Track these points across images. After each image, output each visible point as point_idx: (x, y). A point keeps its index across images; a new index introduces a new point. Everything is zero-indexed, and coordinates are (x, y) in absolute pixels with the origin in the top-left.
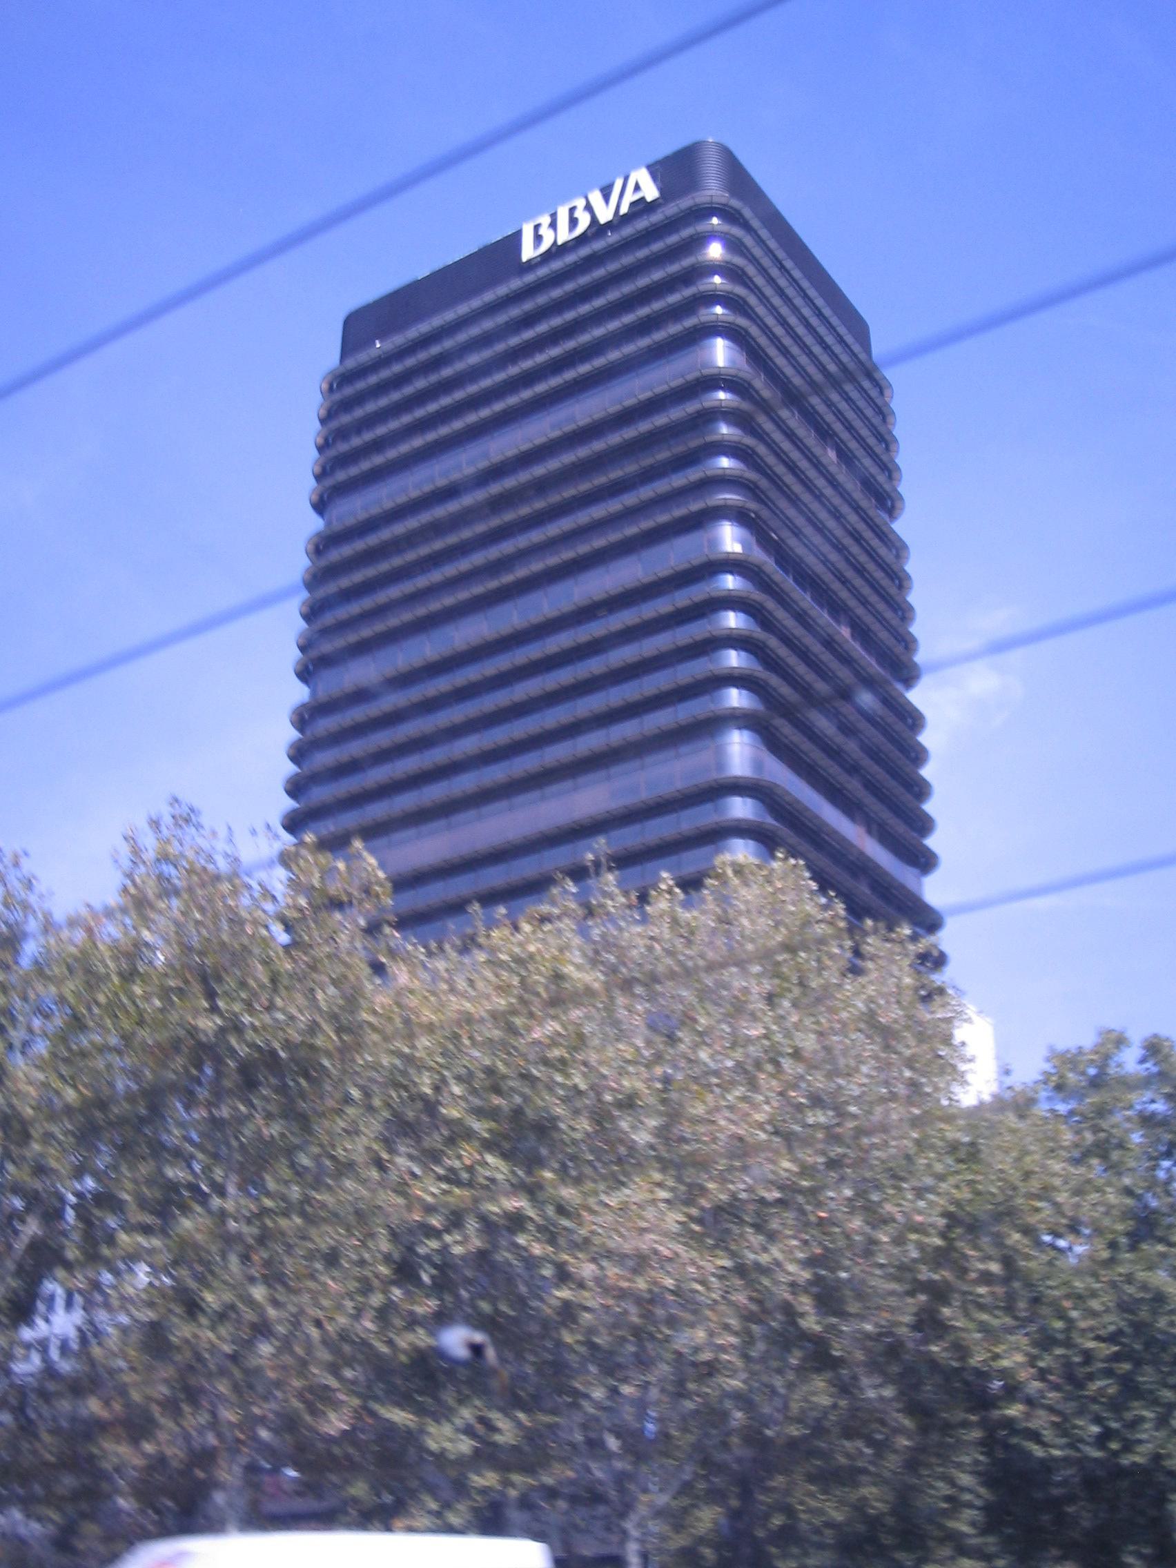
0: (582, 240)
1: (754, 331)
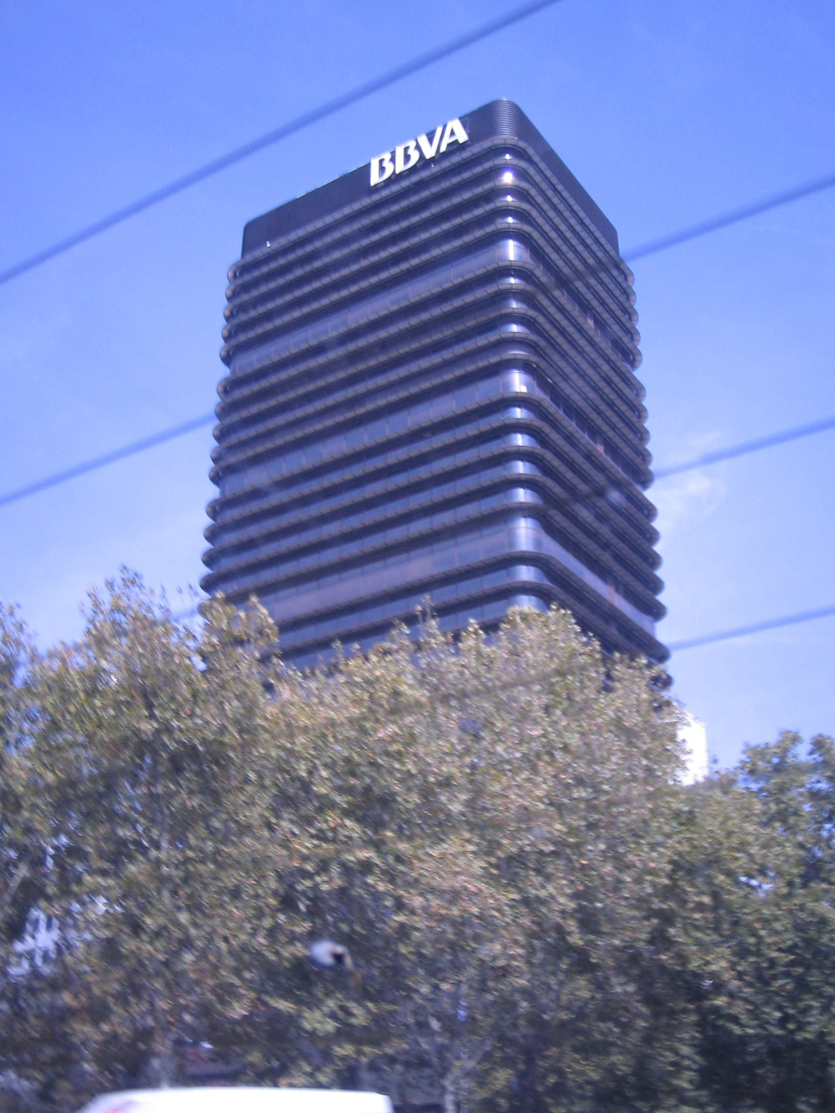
0: (413, 170)
1: (535, 235)
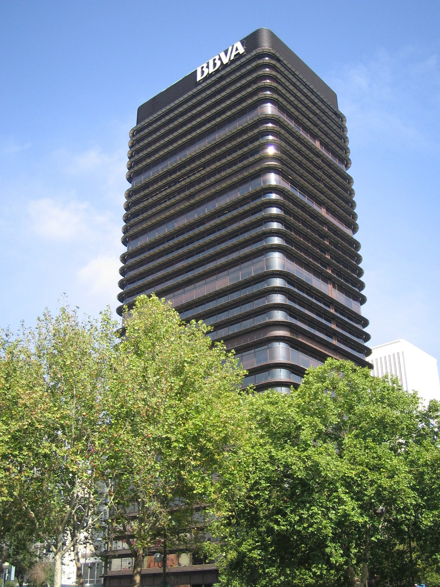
0: (217, 71)
1: (281, 99)
